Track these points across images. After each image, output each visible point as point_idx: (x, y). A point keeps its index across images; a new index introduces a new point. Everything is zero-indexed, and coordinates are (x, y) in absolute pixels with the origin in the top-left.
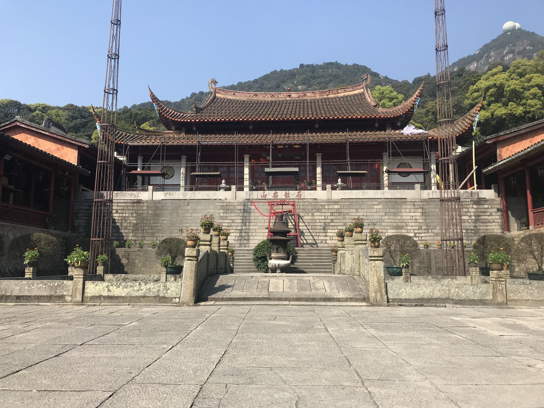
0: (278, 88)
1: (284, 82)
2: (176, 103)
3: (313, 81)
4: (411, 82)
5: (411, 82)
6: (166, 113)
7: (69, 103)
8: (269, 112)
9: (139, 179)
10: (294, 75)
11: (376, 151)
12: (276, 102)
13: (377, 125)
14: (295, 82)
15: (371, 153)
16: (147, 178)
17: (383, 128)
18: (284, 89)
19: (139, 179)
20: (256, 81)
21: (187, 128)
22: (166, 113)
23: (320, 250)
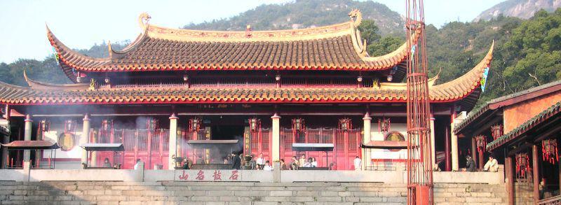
0: (265, 25)
1: (275, 19)
2: (467, 24)
3: (312, 19)
4: (438, 27)
5: (465, 23)
6: (66, 57)
7: (453, 19)
8: (237, 58)
9: (27, 153)
10: (288, 12)
11: (354, 113)
12: (298, 43)
13: (360, 79)
14: (289, 20)
15: (354, 113)
16: (38, 153)
17: (368, 82)
18: (273, 26)
19: (27, 153)
20: (235, 19)
21: (118, 78)
22: (66, 57)
23: (422, 144)
